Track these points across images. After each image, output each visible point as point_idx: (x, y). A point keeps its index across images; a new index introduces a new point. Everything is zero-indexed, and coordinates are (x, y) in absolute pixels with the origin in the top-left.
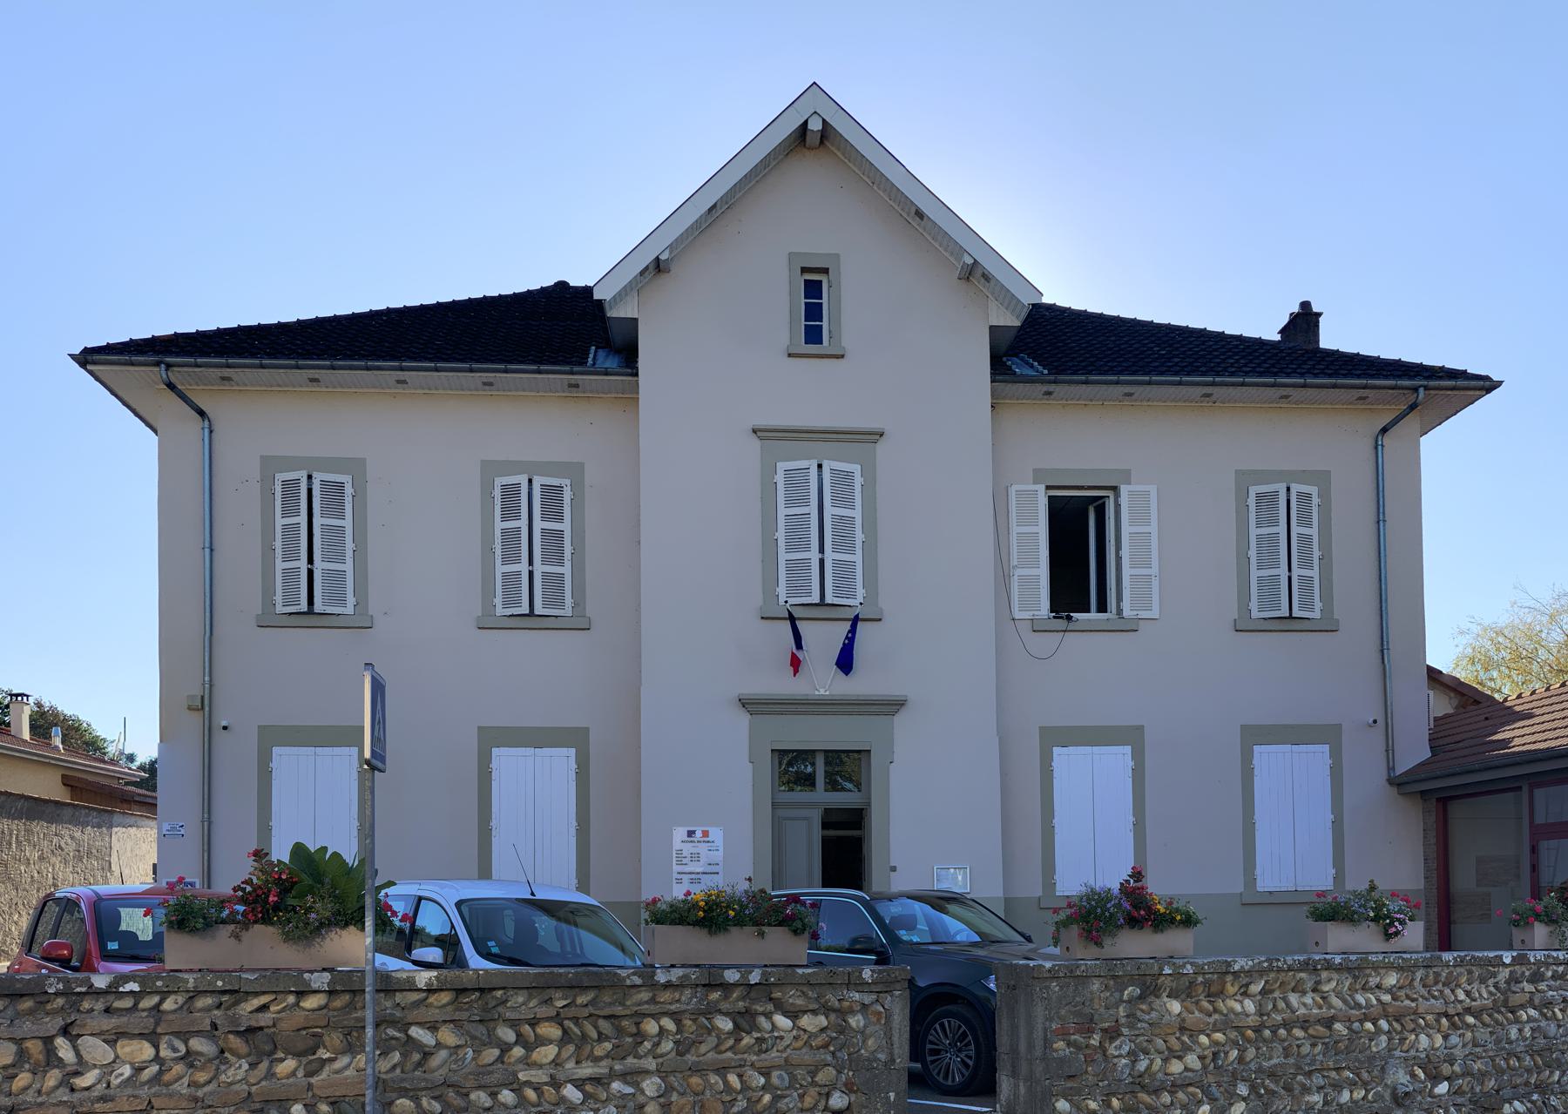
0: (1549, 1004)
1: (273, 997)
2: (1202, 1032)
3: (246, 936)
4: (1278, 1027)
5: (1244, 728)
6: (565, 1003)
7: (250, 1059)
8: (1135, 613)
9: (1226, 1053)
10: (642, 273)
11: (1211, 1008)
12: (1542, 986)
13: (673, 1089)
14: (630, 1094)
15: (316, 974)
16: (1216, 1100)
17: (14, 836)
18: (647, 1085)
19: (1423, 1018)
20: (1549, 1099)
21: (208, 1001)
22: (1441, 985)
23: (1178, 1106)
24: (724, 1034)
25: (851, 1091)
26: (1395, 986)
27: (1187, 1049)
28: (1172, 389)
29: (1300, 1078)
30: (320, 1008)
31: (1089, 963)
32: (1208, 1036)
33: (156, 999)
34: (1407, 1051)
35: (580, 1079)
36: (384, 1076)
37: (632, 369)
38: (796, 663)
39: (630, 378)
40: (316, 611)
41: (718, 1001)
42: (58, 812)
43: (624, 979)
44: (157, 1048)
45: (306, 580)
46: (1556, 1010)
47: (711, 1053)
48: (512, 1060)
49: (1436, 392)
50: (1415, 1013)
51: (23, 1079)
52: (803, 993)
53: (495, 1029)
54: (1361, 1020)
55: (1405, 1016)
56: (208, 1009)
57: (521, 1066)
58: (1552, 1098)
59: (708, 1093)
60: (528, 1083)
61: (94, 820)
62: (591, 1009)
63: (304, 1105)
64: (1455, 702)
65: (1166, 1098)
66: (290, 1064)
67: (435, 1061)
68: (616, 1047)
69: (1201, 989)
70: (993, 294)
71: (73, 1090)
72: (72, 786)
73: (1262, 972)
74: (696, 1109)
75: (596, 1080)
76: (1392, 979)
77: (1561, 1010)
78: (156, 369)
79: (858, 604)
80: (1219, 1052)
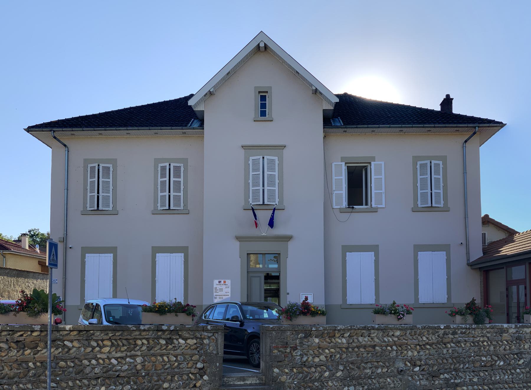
0: (459, 342)
1: (24, 332)
2: (327, 349)
3: (18, 315)
4: (355, 347)
6: (112, 335)
7: (17, 350)
8: (376, 206)
9: (335, 356)
10: (205, 96)
13: (146, 361)
14: (133, 362)
15: (36, 326)
17: (12, 283)
18: (138, 359)
19: (410, 346)
20: (459, 374)
21: (5, 333)
23: (318, 372)
24: (163, 345)
25: (204, 362)
26: (399, 335)
27: (321, 354)
28: (388, 129)
30: (38, 336)
31: (286, 326)
32: (329, 350)
35: (117, 357)
37: (202, 127)
40: (99, 209)
41: (161, 335)
42: (28, 275)
43: (130, 328)
45: (97, 198)
46: (462, 344)
47: (158, 350)
48: (96, 351)
49: (483, 128)
52: (189, 333)
53: (90, 342)
54: (386, 346)
55: (404, 345)
56: (6, 335)
57: (98, 353)
59: (157, 362)
60: (100, 358)
61: (41, 277)
63: (33, 363)
64: (507, 235)
65: (313, 370)
66: (29, 351)
67: (71, 351)
68: (128, 348)
69: (326, 335)
70: (324, 98)
72: (42, 265)
73: (349, 330)
74: (154, 367)
75: (122, 358)
76: (398, 333)
77: (464, 344)
79: (275, 204)
80: (332, 355)
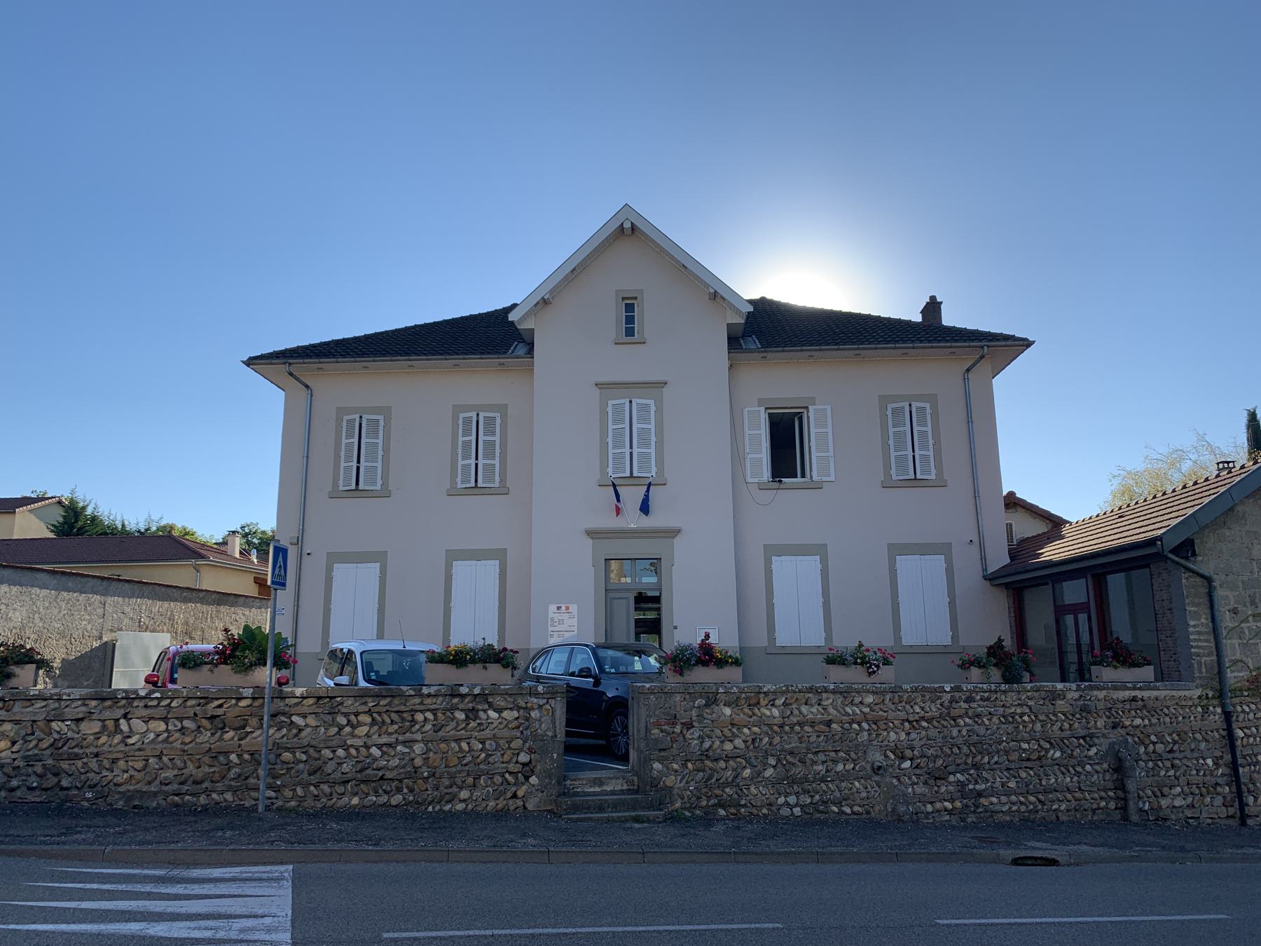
0: (978, 716)
4: (795, 724)
5: (889, 545)
6: (374, 704)
9: (761, 740)
10: (536, 305)
11: (751, 713)
12: (974, 705)
13: (431, 750)
16: (756, 766)
19: (893, 723)
20: (981, 773)
21: (193, 702)
22: (904, 703)
23: (730, 769)
26: (872, 703)
28: (835, 353)
29: (810, 756)
32: (749, 729)
33: (169, 701)
34: (882, 742)
36: (277, 741)
38: (618, 511)
39: (530, 360)
41: (457, 704)
44: (167, 725)
46: (984, 719)
48: (344, 734)
50: (886, 719)
51: (104, 739)
52: (505, 698)
57: (350, 737)
58: (984, 772)
60: (352, 746)
62: (387, 708)
63: (237, 755)
66: (231, 733)
67: (303, 734)
69: (743, 702)
71: (126, 745)
73: (783, 693)
78: (284, 366)
